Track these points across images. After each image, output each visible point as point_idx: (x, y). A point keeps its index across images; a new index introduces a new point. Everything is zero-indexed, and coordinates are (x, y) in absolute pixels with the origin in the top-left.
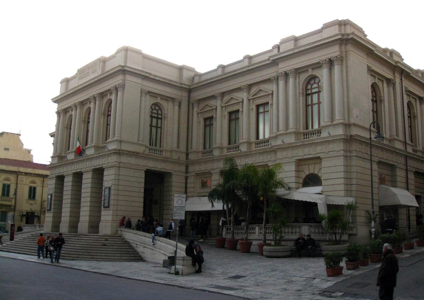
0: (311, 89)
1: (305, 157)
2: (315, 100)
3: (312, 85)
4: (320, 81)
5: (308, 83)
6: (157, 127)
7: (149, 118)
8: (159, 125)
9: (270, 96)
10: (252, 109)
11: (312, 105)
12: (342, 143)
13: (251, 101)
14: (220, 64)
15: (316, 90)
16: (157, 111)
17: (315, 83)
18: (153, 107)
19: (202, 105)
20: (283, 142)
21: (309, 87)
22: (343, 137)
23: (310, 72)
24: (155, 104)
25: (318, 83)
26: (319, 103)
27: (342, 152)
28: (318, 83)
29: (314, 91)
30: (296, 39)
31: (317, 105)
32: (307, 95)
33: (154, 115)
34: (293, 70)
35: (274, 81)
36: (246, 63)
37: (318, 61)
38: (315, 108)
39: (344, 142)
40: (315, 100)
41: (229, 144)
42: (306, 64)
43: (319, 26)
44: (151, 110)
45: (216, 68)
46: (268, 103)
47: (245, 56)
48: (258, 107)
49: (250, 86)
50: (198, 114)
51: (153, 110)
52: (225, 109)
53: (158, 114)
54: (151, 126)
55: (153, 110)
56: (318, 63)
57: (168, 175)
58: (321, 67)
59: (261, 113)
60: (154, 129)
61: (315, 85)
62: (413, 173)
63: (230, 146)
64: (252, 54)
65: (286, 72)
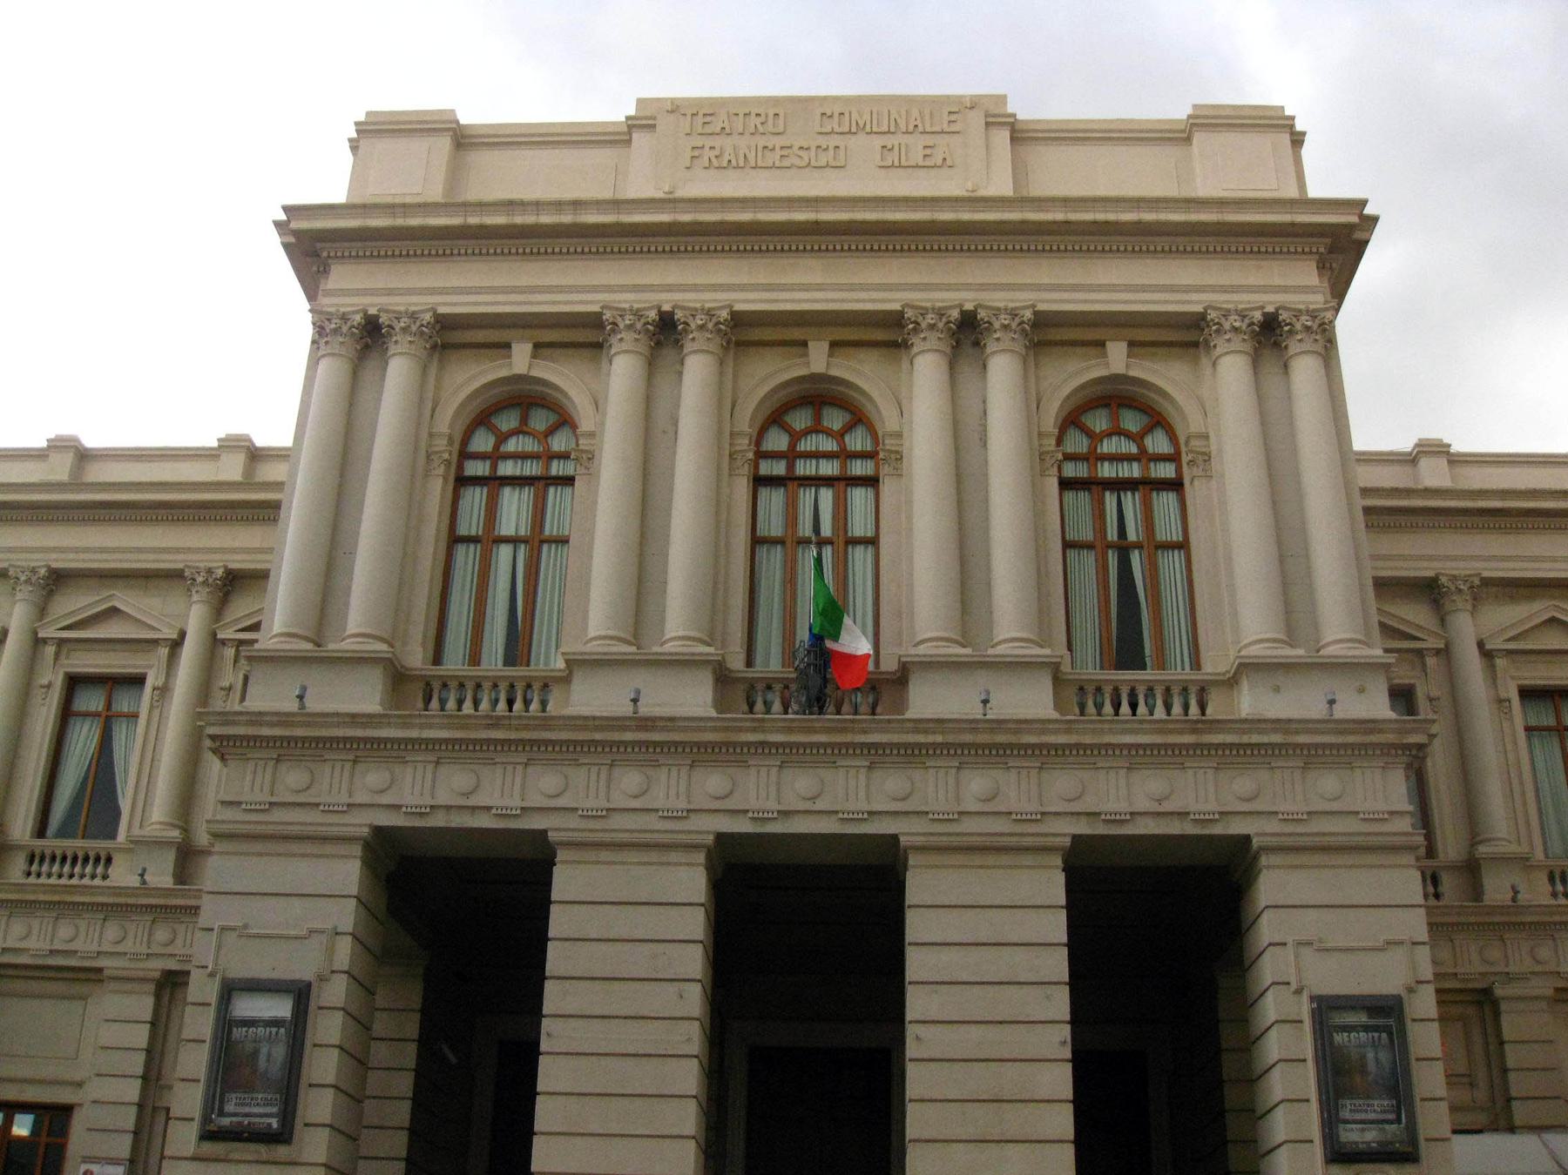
9: (164, 652)
10: (49, 686)
13: (50, 650)
20: (144, 882)
30: (84, 456)
31: (1552, 722)
34: (43, 571)
35: (24, 593)
36: (60, 470)
37: (181, 566)
41: (41, 832)
42: (95, 565)
45: (44, 444)
46: (138, 681)
47: (59, 439)
48: (74, 683)
49: (58, 580)
52: (57, 655)
59: (86, 715)
62: (1544, 1005)
63: (40, 842)
64: (91, 441)
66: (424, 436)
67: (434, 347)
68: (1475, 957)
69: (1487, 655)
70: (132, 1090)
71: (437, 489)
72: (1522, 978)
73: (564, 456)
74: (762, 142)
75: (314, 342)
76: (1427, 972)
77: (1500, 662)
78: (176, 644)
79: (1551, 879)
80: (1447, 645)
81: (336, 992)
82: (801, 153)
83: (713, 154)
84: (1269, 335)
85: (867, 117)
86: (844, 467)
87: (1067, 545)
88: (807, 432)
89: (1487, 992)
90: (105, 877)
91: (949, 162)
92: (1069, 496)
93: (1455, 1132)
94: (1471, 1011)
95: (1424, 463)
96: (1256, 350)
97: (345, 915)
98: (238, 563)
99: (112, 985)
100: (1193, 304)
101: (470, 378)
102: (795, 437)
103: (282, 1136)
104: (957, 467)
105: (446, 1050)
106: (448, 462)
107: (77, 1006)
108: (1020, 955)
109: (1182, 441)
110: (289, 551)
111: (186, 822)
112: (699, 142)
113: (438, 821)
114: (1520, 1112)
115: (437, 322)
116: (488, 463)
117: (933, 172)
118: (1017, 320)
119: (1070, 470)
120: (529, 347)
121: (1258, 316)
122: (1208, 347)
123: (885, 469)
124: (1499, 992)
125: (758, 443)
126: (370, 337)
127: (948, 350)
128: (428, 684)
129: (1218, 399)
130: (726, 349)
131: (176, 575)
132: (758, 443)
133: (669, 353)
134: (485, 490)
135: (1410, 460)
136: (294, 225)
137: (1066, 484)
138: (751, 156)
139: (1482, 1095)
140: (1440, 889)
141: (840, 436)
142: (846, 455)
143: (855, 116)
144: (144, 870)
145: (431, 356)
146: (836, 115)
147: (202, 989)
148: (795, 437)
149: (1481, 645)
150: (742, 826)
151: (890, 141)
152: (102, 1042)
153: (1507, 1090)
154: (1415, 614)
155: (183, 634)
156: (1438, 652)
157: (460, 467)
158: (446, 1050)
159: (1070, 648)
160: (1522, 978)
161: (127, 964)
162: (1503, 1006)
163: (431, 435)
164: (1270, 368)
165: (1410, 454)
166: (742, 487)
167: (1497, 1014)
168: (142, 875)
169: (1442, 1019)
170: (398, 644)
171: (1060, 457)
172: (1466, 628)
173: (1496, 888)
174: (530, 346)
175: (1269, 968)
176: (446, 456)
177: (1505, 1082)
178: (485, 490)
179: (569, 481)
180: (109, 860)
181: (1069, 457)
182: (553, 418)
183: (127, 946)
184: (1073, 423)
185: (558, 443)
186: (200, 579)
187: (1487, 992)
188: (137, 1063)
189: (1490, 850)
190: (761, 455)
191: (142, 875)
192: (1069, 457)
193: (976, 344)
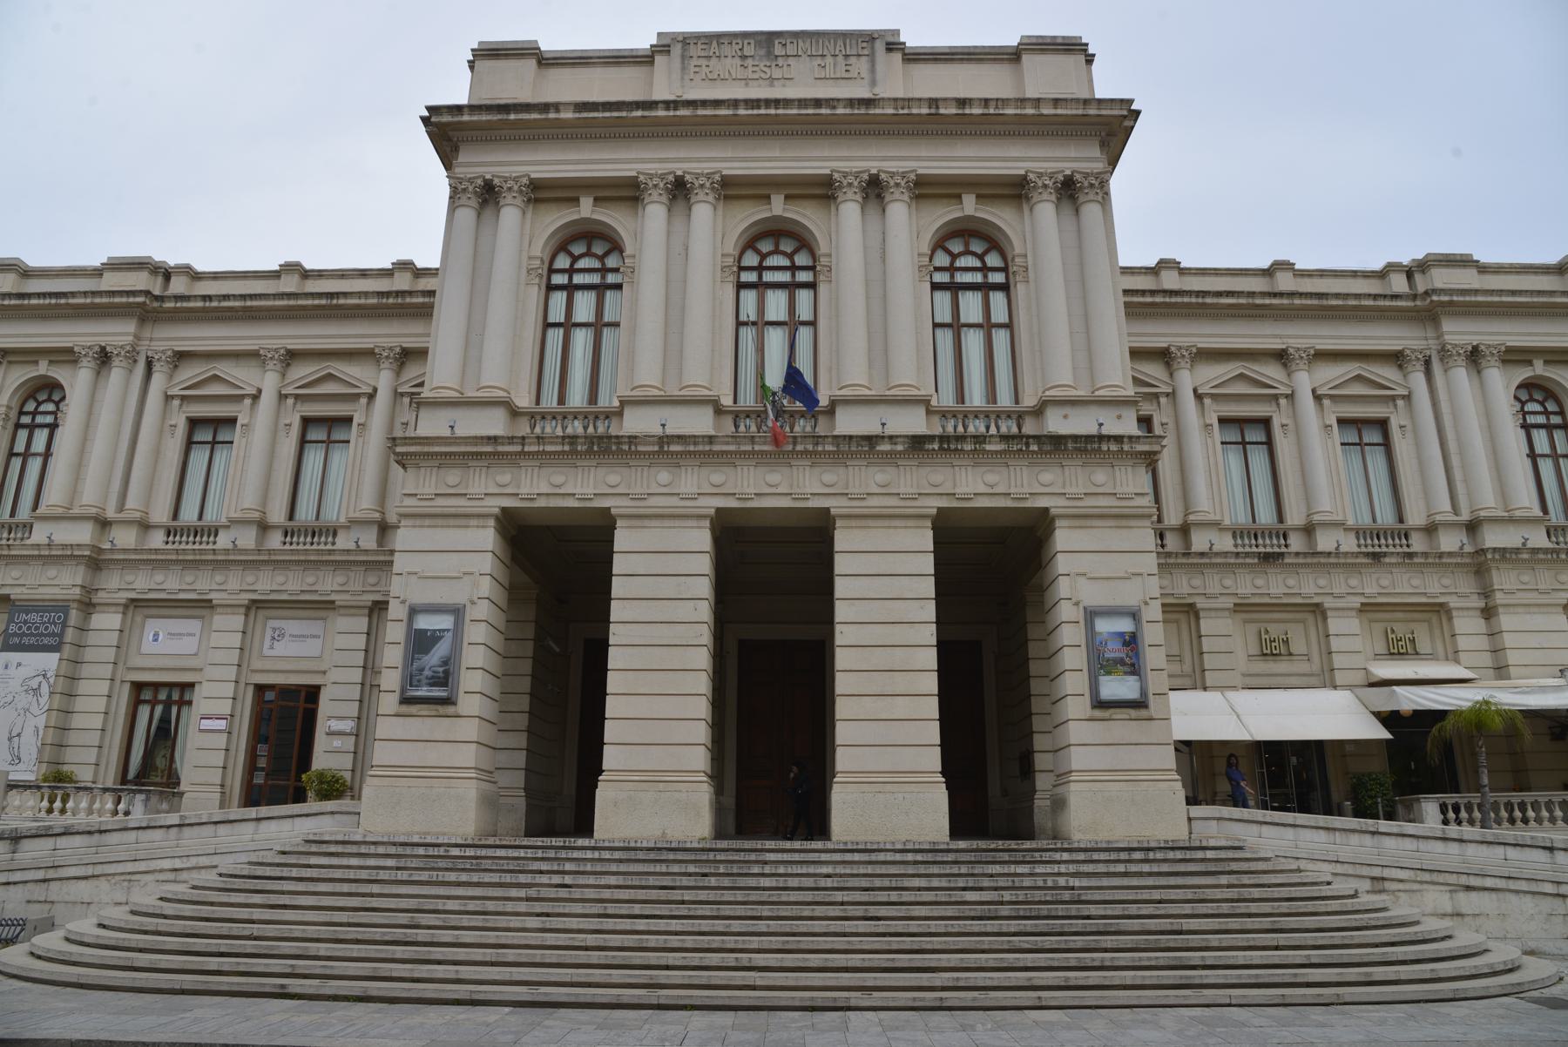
0: (34, 414)
1: (182, 596)
2: (39, 444)
3: (39, 404)
4: (64, 398)
5: (31, 395)
6: (987, 326)
7: (1522, 433)
8: (804, 313)
11: (26, 455)
12: (82, 569)
14: (292, 258)
15: (49, 419)
16: (981, 257)
17: (49, 400)
18: (1524, 397)
19: (190, 373)
21: (30, 406)
22: (87, 553)
23: (43, 368)
24: (1526, 385)
25: (57, 404)
26: (47, 455)
27: (77, 591)
28: (57, 404)
29: (39, 419)
32: (18, 426)
33: (1531, 420)
38: (35, 465)
39: (88, 566)
40: (39, 444)
43: (96, 260)
44: (1518, 406)
50: (168, 398)
51: (1523, 403)
53: (985, 269)
54: (1533, 456)
55: (1523, 403)
56: (70, 351)
57: (742, 644)
58: (75, 362)
60: (1546, 467)
61: (51, 407)
65: (103, 349)
67: (529, 200)
71: (534, 294)
73: (616, 270)
84: (1069, 190)
87: (936, 325)
95: (1164, 274)
97: (487, 563)
99: (342, 611)
113: (542, 503)
114: (1210, 678)
122: (1028, 199)
139: (1187, 667)
154: (1154, 371)
166: (730, 290)
175: (1063, 588)
179: (618, 287)
181: (937, 269)
188: (359, 658)
192: (937, 269)
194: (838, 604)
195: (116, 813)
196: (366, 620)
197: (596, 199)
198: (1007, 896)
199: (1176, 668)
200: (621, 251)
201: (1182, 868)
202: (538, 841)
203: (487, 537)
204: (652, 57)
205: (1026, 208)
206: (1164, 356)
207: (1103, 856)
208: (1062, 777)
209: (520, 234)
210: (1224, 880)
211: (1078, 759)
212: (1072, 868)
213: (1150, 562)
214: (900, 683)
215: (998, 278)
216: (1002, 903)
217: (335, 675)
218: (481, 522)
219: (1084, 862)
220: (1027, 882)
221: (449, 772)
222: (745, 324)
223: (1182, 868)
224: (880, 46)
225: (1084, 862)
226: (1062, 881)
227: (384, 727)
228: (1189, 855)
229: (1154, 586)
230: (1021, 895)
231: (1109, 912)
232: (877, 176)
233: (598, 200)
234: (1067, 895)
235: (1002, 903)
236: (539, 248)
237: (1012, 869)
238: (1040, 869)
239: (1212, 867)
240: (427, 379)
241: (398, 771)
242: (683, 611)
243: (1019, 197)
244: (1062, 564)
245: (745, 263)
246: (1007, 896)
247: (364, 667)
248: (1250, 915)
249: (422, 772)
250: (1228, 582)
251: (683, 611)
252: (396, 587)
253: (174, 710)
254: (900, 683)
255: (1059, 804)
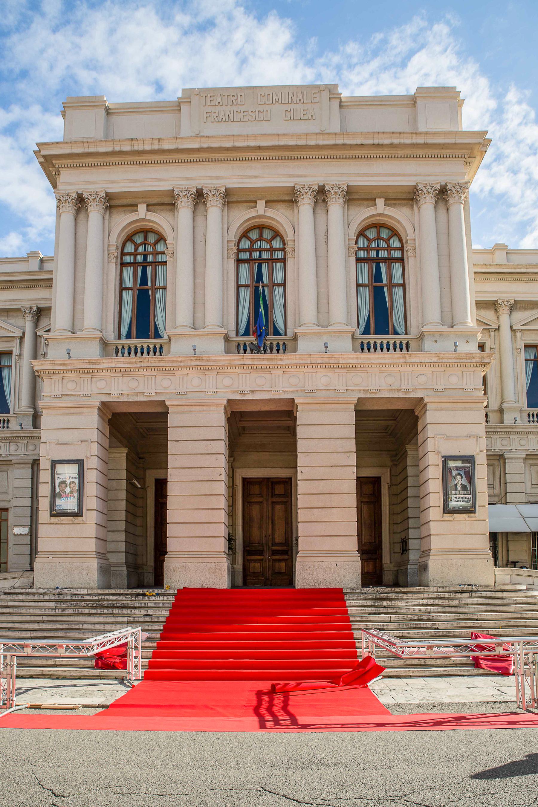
20: (22, 428)
37: (20, 307)
57: (244, 479)
66: (106, 246)
67: (106, 208)
68: (499, 443)
69: (512, 330)
70: (28, 502)
71: (113, 268)
72: (515, 451)
73: (163, 253)
74: (235, 108)
75: (58, 207)
76: (484, 448)
77: (518, 334)
78: (22, 338)
79: (529, 415)
80: (499, 327)
81: (93, 465)
82: (251, 114)
83: (215, 115)
84: (443, 194)
85: (279, 96)
86: (271, 254)
87: (358, 285)
88: (257, 240)
89: (502, 456)
90: (8, 427)
91: (314, 118)
92: (359, 265)
93: (489, 504)
94: (496, 463)
95: (497, 253)
96: (436, 201)
97: (95, 435)
98: (42, 304)
99: (17, 466)
100: (410, 182)
101: (123, 221)
102: (253, 242)
103: (79, 514)
104: (316, 254)
105: (136, 482)
106: (117, 257)
107: (5, 474)
108: (339, 442)
109: (404, 242)
110: (60, 300)
111: (34, 405)
112: (209, 109)
113: (124, 399)
114: (510, 498)
115: (107, 196)
116: (132, 257)
117: (307, 121)
118: (341, 190)
119: (361, 254)
120: (145, 205)
121: (438, 187)
122: (417, 202)
123: (289, 255)
124: (506, 456)
125: (238, 246)
126: (81, 202)
127: (313, 203)
128: (117, 347)
129: (419, 224)
130: (224, 205)
131: (19, 310)
132: (238, 246)
133: (201, 208)
134: (132, 268)
135: (491, 252)
136: (43, 153)
137: (358, 260)
138: (231, 116)
139: (497, 491)
140: (488, 419)
141: (270, 241)
142: (272, 250)
143: (274, 96)
144: (22, 424)
145: (105, 211)
146: (265, 111)
147: (45, 464)
148: (253, 242)
149: (511, 327)
150: (238, 397)
151: (288, 107)
152: (16, 486)
153: (506, 489)
154: (488, 315)
155: (24, 334)
156: (496, 330)
157: (122, 259)
158: (136, 482)
159: (358, 327)
160: (515, 451)
161: (18, 458)
162: (507, 461)
163: (109, 246)
164: (442, 208)
165: (491, 250)
166: (232, 264)
167: (505, 463)
168: (21, 426)
169: (488, 465)
170: (104, 332)
171: (357, 249)
172: (505, 320)
173: (508, 418)
174: (145, 205)
175: (430, 445)
176: (116, 255)
177: (506, 487)
178: (132, 268)
179: (164, 263)
180: (8, 421)
181: (359, 249)
182: (157, 237)
183: (19, 452)
184: (362, 234)
185: (160, 247)
186: (28, 312)
187: (502, 456)
188: (28, 493)
189: (507, 405)
190: (239, 250)
191: (21, 426)
192: (359, 249)
193: (324, 200)
194: (299, 456)
195: (4, 427)
196: (30, 471)
197: (148, 205)
198: (393, 617)
199: (492, 491)
200: (165, 241)
201: (490, 601)
202: (133, 591)
203: (93, 420)
204: (180, 106)
205: (415, 207)
206: (493, 305)
207: (446, 595)
208: (426, 553)
209: (101, 234)
210: (513, 607)
211: (435, 543)
212: (429, 602)
213: (481, 429)
214: (336, 500)
215: (397, 254)
216: (390, 621)
217: (15, 502)
218: (90, 410)
219: (437, 598)
220: (404, 610)
221: (81, 555)
222: (242, 286)
223: (490, 601)
224: (325, 95)
225: (437, 598)
226: (423, 609)
227: (43, 530)
228: (494, 594)
229: (483, 444)
230: (401, 617)
231: (449, 625)
232: (324, 186)
233: (150, 207)
234: (426, 617)
235: (390, 621)
236: (115, 240)
237: (396, 602)
238: (411, 603)
239: (506, 601)
240: (51, 327)
241: (53, 555)
242: (210, 461)
243: (412, 199)
244: (430, 431)
245: (242, 246)
246: (393, 617)
247: (32, 498)
248: (526, 627)
249: (65, 555)
250: (523, 442)
251: (210, 461)
252: (43, 450)
253: (149, 270)
254: (336, 500)
255: (424, 568)
